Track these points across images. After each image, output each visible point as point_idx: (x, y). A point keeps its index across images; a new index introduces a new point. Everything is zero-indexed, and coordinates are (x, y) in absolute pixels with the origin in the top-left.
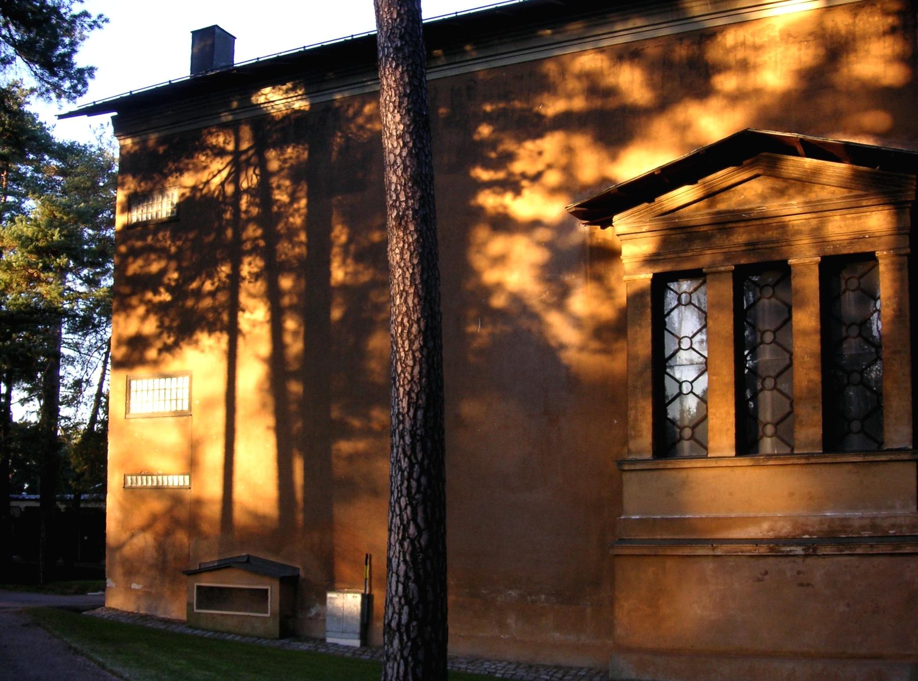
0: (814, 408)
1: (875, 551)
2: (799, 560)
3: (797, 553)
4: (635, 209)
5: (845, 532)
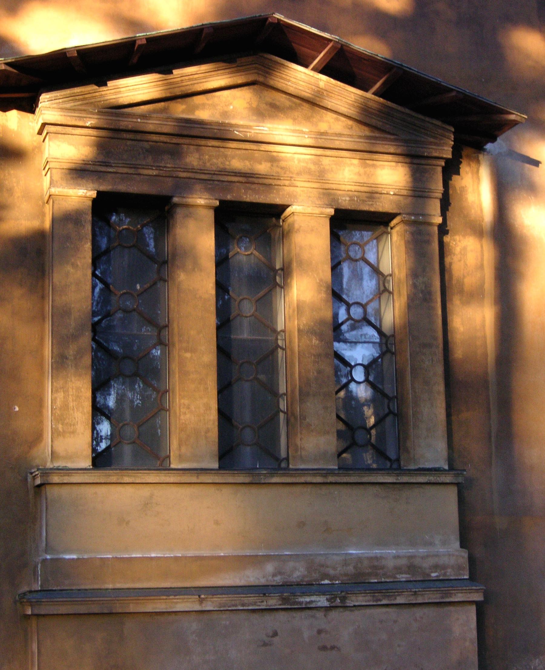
0: (325, 408)
1: (420, 600)
2: (320, 614)
3: (319, 604)
4: (77, 90)
5: (376, 575)
